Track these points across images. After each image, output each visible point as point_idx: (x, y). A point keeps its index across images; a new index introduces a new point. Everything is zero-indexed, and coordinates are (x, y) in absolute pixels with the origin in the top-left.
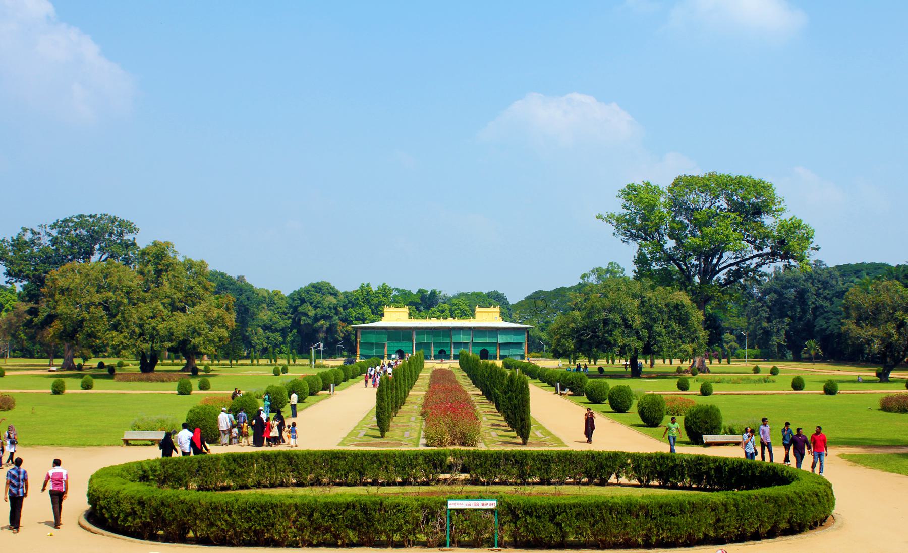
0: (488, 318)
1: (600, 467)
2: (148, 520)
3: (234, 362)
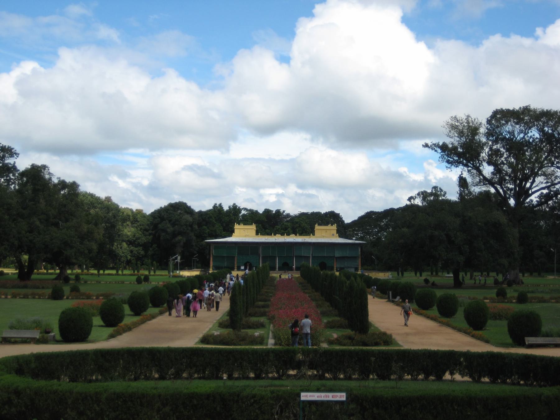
0: (325, 235)
1: (436, 363)
2: (23, 409)
3: (101, 272)
